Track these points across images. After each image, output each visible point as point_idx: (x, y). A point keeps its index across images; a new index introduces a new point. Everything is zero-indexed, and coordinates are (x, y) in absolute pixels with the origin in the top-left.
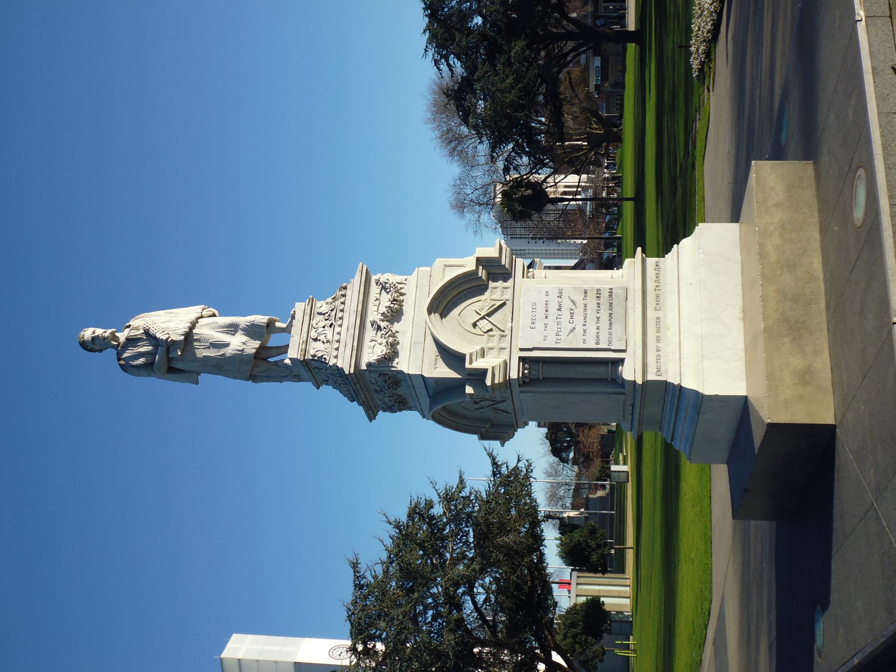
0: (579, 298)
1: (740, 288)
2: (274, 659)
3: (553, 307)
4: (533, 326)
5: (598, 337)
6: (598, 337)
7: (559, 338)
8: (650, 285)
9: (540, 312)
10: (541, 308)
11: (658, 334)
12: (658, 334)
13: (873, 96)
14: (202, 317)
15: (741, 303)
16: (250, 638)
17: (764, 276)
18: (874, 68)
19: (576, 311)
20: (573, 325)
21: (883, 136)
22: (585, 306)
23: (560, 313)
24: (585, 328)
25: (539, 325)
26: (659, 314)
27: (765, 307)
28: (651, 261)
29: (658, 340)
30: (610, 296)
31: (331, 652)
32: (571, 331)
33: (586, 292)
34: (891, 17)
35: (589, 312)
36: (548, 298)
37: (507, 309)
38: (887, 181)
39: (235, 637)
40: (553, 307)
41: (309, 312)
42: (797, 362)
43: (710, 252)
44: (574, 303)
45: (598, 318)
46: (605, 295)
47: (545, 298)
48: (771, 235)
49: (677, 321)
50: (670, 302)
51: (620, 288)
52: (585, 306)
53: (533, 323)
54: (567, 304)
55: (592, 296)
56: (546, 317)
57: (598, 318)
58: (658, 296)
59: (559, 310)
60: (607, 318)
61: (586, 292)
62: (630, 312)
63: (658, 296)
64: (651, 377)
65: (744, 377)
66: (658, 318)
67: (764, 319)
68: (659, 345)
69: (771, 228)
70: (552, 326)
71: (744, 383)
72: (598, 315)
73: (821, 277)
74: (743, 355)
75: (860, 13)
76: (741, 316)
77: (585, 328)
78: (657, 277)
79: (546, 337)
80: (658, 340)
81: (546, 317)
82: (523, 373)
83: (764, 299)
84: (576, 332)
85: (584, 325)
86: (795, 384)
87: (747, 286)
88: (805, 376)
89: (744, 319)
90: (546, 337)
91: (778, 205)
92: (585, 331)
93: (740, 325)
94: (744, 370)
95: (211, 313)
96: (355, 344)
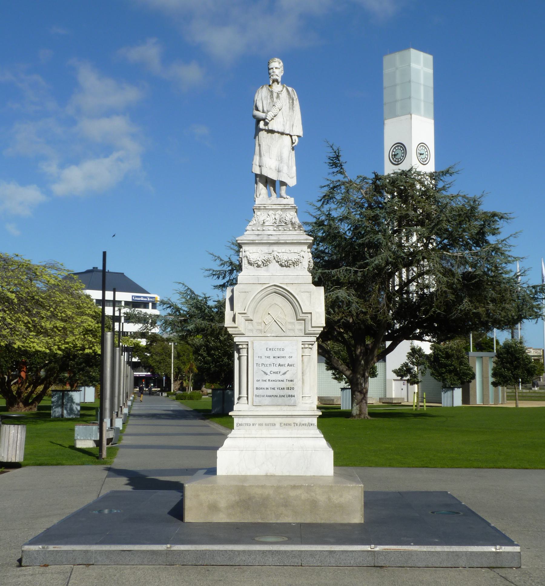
0: (288, 376)
1: (288, 474)
2: (412, 95)
3: (281, 361)
4: (268, 349)
5: (261, 388)
6: (261, 388)
7: (261, 365)
8: (298, 420)
9: (277, 353)
10: (281, 354)
11: (264, 425)
12: (264, 425)
13: (314, 549)
14: (291, 136)
15: (277, 475)
16: (430, 71)
17: (279, 487)
18: (334, 552)
19: (279, 375)
20: (269, 373)
21: (285, 552)
22: (283, 381)
23: (277, 365)
24: (267, 381)
25: (269, 353)
26: (278, 425)
27: (258, 486)
28: (315, 421)
29: (260, 425)
30: (289, 396)
31: (422, 145)
32: (265, 373)
33: (291, 381)
34: (374, 566)
35: (278, 383)
36: (287, 358)
37: (281, 333)
38: (253, 551)
39: (430, 58)
40: (281, 361)
41: (286, 208)
42: (223, 504)
43: (312, 456)
44: (285, 374)
45: (274, 389)
46: (290, 392)
47: (287, 356)
48: (307, 493)
49: (270, 436)
50: (265, 432)
51: (295, 401)
52: (283, 381)
53: (270, 349)
54: (283, 369)
55: (290, 384)
56: (274, 357)
57: (274, 389)
58: (290, 425)
59: (279, 365)
60: (274, 394)
61: (291, 381)
62: (279, 408)
63: (290, 425)
64: (236, 421)
65: (229, 474)
66: (275, 425)
67: (250, 486)
68: (257, 425)
69: (313, 494)
70: (268, 361)
71: (224, 474)
72: (276, 389)
73: (279, 522)
74: (243, 474)
75: (378, 548)
76: (269, 474)
77: (267, 381)
78: (303, 425)
79: (261, 357)
80: (260, 425)
81: (274, 357)
82: (240, 345)
83: (263, 487)
84: (265, 375)
85: (269, 380)
86: (209, 501)
87: (267, 477)
88: (214, 508)
89: (267, 476)
90: (261, 357)
91: (329, 499)
92: (265, 381)
93: (263, 473)
94: (233, 474)
95: (294, 141)
96: (257, 242)
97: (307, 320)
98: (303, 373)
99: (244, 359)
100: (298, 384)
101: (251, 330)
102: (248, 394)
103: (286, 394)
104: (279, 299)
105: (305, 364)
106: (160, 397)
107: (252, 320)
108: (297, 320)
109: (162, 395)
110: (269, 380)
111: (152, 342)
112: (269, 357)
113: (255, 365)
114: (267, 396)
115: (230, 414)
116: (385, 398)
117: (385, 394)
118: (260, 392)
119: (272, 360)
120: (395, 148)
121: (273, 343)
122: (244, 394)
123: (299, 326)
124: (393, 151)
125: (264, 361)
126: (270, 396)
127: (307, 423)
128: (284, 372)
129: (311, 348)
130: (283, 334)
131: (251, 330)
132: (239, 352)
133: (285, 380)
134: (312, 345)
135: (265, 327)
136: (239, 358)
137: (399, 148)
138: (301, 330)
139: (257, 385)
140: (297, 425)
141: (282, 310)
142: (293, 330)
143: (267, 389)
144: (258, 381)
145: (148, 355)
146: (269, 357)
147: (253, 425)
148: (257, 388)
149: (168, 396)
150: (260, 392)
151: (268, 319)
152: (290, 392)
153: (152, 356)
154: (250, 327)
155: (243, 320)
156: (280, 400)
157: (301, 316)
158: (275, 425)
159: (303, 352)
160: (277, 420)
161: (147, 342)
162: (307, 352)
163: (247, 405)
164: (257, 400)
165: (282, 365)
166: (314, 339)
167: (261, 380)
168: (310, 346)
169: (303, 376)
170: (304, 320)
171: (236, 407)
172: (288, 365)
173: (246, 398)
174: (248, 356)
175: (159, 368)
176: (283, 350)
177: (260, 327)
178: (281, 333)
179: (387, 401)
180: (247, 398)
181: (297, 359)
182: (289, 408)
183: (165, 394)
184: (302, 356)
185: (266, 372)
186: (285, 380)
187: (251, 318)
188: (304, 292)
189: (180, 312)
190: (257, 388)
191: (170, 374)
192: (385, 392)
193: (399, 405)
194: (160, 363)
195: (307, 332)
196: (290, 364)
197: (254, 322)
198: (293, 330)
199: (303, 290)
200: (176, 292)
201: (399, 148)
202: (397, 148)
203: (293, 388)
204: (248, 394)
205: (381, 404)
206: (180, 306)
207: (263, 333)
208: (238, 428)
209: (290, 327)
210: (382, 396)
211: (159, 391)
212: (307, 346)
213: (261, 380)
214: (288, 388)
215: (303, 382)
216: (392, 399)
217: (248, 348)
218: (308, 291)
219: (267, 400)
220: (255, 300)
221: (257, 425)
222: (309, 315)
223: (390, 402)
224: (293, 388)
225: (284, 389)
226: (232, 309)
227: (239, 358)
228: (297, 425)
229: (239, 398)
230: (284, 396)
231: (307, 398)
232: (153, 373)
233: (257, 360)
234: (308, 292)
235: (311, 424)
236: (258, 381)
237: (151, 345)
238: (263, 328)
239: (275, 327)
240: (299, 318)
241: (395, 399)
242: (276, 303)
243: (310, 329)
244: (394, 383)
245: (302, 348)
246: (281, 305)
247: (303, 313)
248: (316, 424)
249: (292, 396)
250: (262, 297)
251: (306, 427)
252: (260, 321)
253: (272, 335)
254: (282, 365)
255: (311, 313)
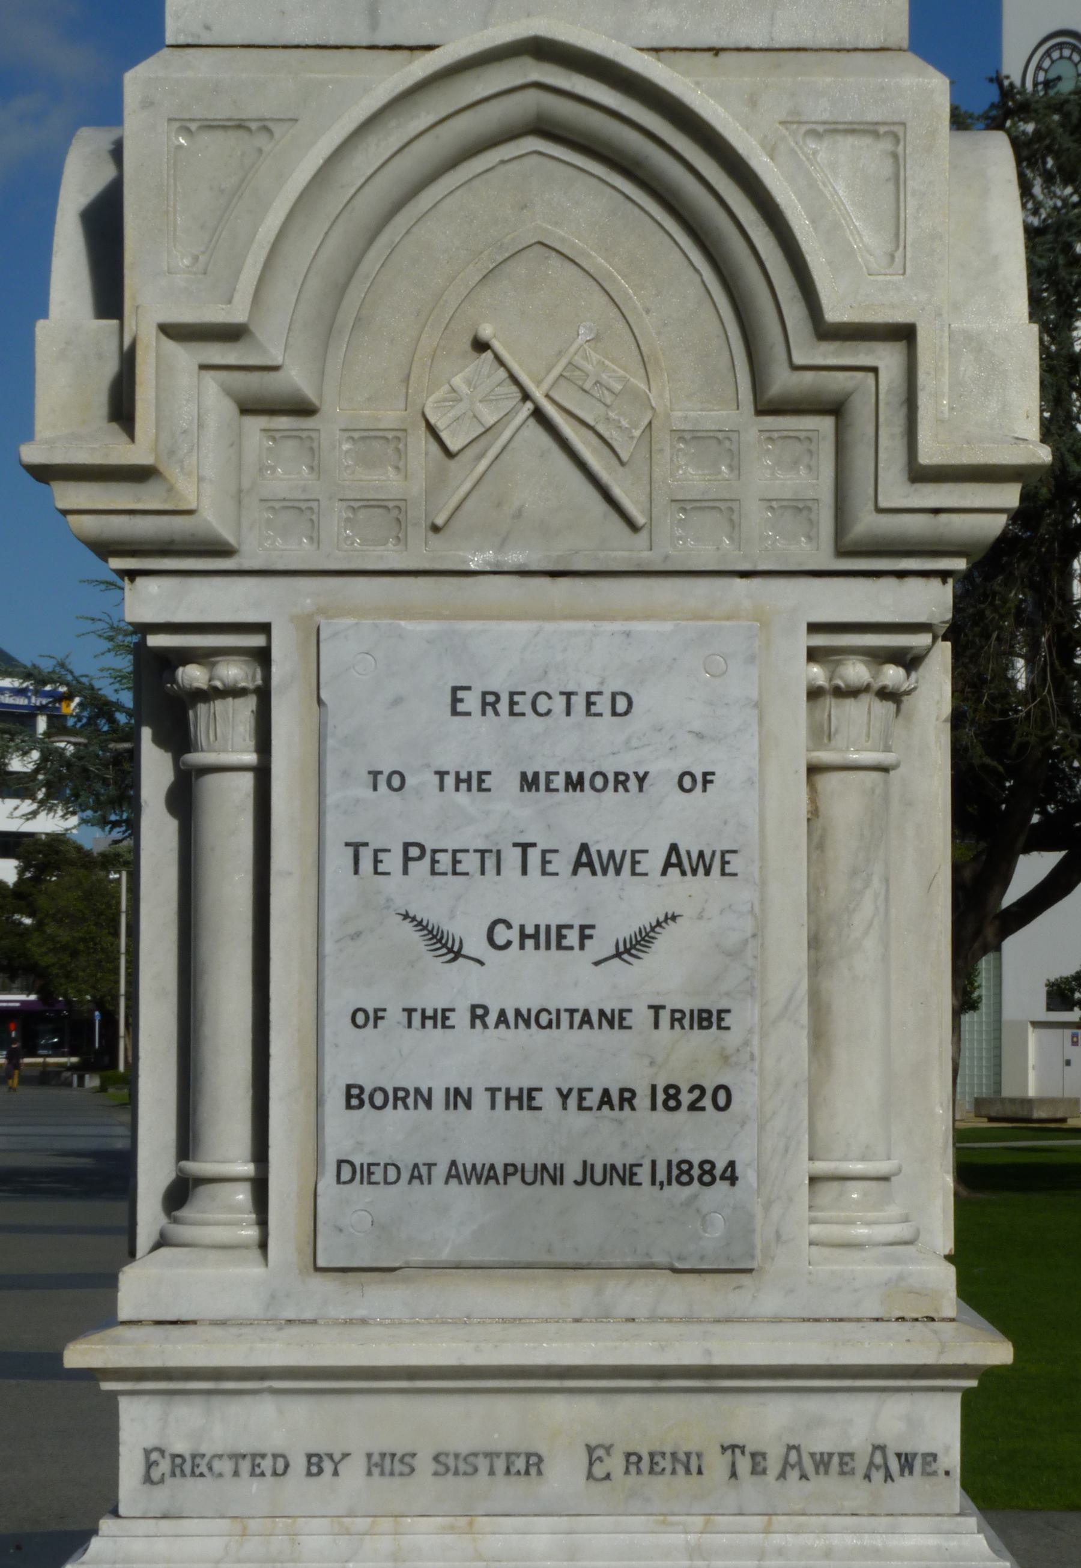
0: (667, 975)
3: (600, 820)
4: (471, 702)
6: (399, 1097)
7: (392, 862)
8: (769, 1420)
9: (562, 745)
10: (600, 744)
11: (424, 1465)
12: (424, 1465)
19: (577, 963)
20: (476, 945)
22: (615, 1019)
23: (561, 864)
24: (460, 1018)
25: (475, 742)
26: (564, 1473)
29: (389, 1464)
30: (682, 1172)
36: (662, 787)
37: (601, 541)
40: (600, 820)
45: (526, 1099)
46: (694, 1137)
47: (664, 767)
52: (615, 1019)
53: (489, 702)
54: (621, 905)
55: (686, 1056)
56: (529, 782)
57: (526, 1099)
58: (688, 1464)
60: (530, 1156)
61: (706, 1019)
62: (578, 1293)
63: (688, 1464)
64: (139, 1424)
68: (354, 1471)
70: (475, 821)
72: (548, 1099)
77: (460, 1018)
78: (822, 1462)
79: (397, 782)
80: (389, 1464)
81: (529, 782)
82: (187, 656)
84: (435, 964)
90: (397, 782)
92: (441, 1018)
97: (861, 414)
98: (815, 942)
99: (228, 802)
100: (769, 1052)
101: (302, 511)
102: (260, 1153)
103: (643, 1157)
104: (579, 204)
105: (844, 847)
106: (74, 1093)
107: (304, 409)
108: (766, 408)
109: (81, 1082)
110: (478, 1015)
111: (42, 870)
112: (475, 781)
113: (338, 860)
114: (454, 1173)
115: (79, 1355)
116: (997, 1097)
117: (998, 1084)
118: (388, 1134)
119: (506, 813)
120: (1048, 53)
121: (512, 643)
122: (227, 1151)
123: (785, 469)
124: (1039, 67)
125: (427, 814)
126: (486, 1175)
127: (858, 1441)
128: (627, 930)
129: (887, 694)
130: (626, 550)
131: (302, 511)
132: (178, 739)
133: (640, 1017)
134: (910, 661)
135: (436, 485)
136: (183, 800)
137: (1067, 53)
138: (800, 507)
139: (355, 1059)
140: (758, 1470)
141: (612, 307)
142: (725, 509)
143: (458, 1098)
144: (366, 1018)
145: (28, 921)
146: (475, 781)
147: (315, 1464)
148: (355, 1097)
149: (103, 1089)
150: (388, 1134)
151: (466, 401)
152: (694, 1137)
153: (39, 926)
154: (288, 476)
155: (215, 398)
156: (591, 1213)
157: (806, 364)
158: (533, 1464)
159: (821, 734)
160: (563, 1422)
161: (21, 872)
162: (857, 728)
163: (255, 1270)
164: (352, 1209)
165: (612, 864)
166: (934, 601)
167: (395, 1015)
168: (893, 675)
169: (817, 967)
170: (836, 409)
171: (138, 1287)
172: (673, 860)
173: (242, 1195)
174: (263, 774)
175: (68, 976)
176: (622, 706)
177: (387, 481)
178: (601, 541)
179: (1010, 1111)
180: (260, 1187)
181: (760, 799)
182: (679, 1295)
183: (92, 1081)
184: (814, 770)
185: (454, 928)
186: (640, 1017)
187: (296, 377)
188: (835, 129)
189: (112, 720)
190: (355, 1097)
191: (116, 998)
192: (998, 1074)
193: (1055, 1127)
194: (74, 954)
195: (867, 523)
196: (689, 845)
197: (328, 426)
198: (725, 509)
199: (821, 111)
200: (89, 626)
201: (1067, 53)
202: (1056, 55)
203: (722, 1098)
204: (260, 1153)
205: (984, 1124)
206: (108, 690)
207: (417, 534)
208: (161, 1498)
209: (691, 476)
210: (985, 1092)
211: (73, 1068)
212: (856, 672)
213: (395, 1015)
214: (672, 1093)
215: (819, 1036)
216: (1027, 1102)
217: (264, 695)
218: (872, 115)
219: (458, 1218)
220: (333, 202)
221: (354, 1471)
222: (887, 358)
223: (1023, 1113)
224: (722, 1098)
225: (627, 1097)
226: (109, 299)
227: (183, 800)
228: (758, 1470)
229: (179, 1194)
230: (627, 1176)
231: (855, 1192)
232: (46, 996)
233: (359, 811)
234: (871, 130)
235: (907, 1462)
236: (366, 1018)
237: (36, 880)
238: (416, 488)
239: (539, 479)
240: (783, 381)
241: (1042, 1101)
242: (560, 234)
243: (893, 500)
244: (1032, 1037)
245: (814, 694)
246: (598, 261)
247: (827, 332)
248: (952, 1458)
249: (707, 1169)
250: (408, 165)
251: (854, 1492)
252: (390, 416)
253: (514, 558)
254: (612, 864)
255: (904, 334)
